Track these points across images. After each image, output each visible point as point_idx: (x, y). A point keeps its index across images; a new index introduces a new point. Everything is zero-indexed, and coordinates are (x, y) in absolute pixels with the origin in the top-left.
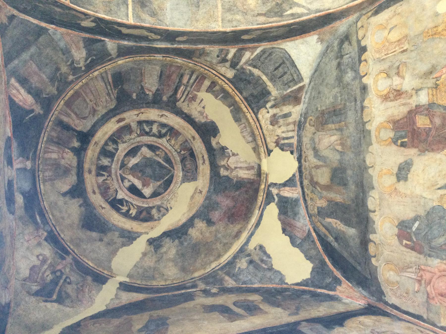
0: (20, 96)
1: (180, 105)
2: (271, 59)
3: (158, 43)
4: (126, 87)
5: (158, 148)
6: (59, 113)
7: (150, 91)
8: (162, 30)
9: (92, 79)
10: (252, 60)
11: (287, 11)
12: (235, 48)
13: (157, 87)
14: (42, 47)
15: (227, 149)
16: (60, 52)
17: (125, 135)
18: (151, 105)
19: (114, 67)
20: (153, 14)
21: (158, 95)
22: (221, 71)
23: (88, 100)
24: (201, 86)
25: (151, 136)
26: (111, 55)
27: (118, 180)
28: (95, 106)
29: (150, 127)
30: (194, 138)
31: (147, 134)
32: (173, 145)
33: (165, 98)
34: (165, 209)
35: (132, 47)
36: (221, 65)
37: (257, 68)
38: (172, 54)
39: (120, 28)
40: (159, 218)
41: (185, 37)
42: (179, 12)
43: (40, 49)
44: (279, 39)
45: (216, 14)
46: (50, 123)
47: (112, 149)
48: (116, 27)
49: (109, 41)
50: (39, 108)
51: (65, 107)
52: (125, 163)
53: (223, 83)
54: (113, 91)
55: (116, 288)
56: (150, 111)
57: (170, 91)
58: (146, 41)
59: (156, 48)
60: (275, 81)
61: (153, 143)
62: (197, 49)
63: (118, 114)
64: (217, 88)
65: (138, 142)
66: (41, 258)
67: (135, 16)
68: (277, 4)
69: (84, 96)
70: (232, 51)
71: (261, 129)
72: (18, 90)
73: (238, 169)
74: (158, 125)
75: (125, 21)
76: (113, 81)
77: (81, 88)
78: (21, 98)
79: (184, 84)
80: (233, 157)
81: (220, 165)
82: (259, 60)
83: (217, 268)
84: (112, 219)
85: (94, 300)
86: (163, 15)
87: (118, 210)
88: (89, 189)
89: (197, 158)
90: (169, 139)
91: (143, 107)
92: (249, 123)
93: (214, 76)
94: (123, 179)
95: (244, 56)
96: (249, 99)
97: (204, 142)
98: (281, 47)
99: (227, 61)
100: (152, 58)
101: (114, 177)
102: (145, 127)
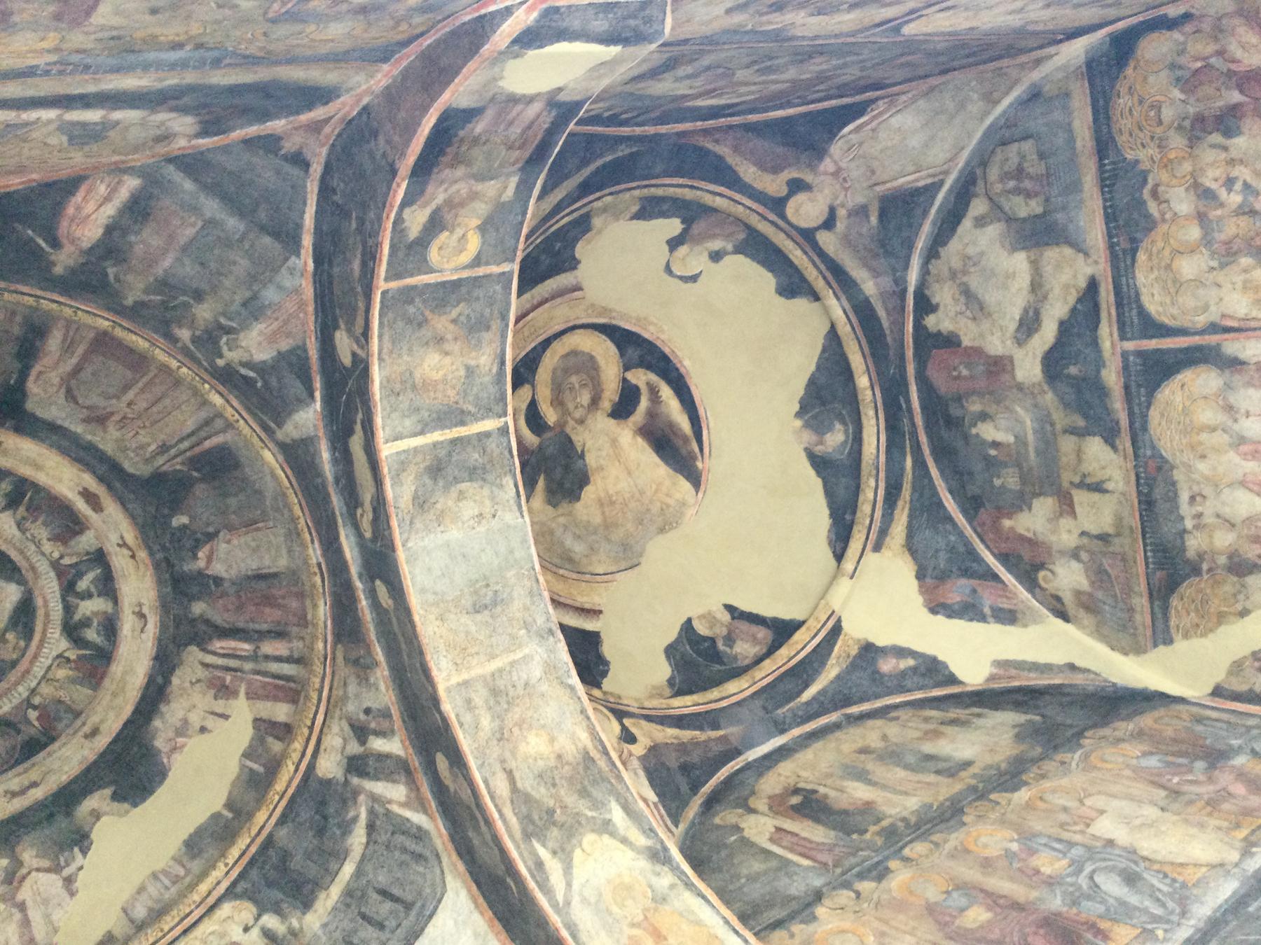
1: (191, 659)
2: (407, 865)
3: (352, 539)
4: (200, 490)
5: (28, 634)
6: (69, 323)
7: (209, 559)
8: (390, 534)
9: (196, 392)
10: (388, 813)
11: (544, 846)
12: (405, 748)
13: (224, 575)
15: (84, 852)
16: (248, 294)
17: (45, 524)
18: (167, 576)
19: (247, 442)
20: (421, 503)
21: (206, 584)
22: (329, 737)
23: (130, 395)
24: (267, 697)
25: (64, 599)
26: (280, 425)
28: (116, 418)
29: (93, 589)
30: (95, 732)
31: (69, 588)
32: (50, 676)
33: (198, 608)
35: (320, 474)
36: (347, 728)
37: (369, 835)
38: (335, 585)
39: (358, 427)
41: (390, 602)
42: (447, 566)
43: (241, 240)
44: (466, 863)
45: (475, 662)
46: (31, 299)
48: (360, 416)
49: (315, 411)
50: (71, 262)
51: (92, 335)
53: (295, 756)
54: (179, 460)
56: (144, 576)
57: (226, 615)
58: (347, 505)
59: (337, 538)
60: (348, 906)
61: (40, 613)
62: (368, 648)
63: (110, 487)
64: (276, 746)
65: (33, 568)
67: (403, 457)
68: (551, 812)
69: (140, 385)
70: (393, 746)
71: (185, 932)
72: (107, 199)
73: (18, 916)
74: (105, 613)
75: (380, 435)
76: (208, 452)
77: (165, 368)
79: (258, 647)
80: (60, 883)
81: (18, 849)
82: (393, 833)
86: (426, 527)
89: (26, 765)
90: (68, 660)
91: (151, 554)
92: (192, 887)
93: (309, 723)
95: (390, 785)
96: (271, 852)
97: (88, 770)
98: (449, 879)
99: (363, 742)
100: (307, 536)
102: (90, 576)
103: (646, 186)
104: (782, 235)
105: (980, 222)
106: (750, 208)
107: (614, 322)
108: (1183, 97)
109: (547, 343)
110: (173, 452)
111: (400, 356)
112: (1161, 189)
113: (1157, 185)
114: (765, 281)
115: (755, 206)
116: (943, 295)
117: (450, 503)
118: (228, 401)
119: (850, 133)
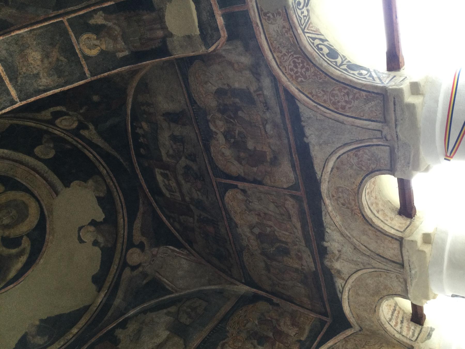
103: (115, 186)
104: (119, 256)
105: (168, 314)
106: (124, 236)
107: (47, 219)
108: (257, 323)
109: (27, 190)
111: (34, 40)
112: (227, 345)
113: (226, 343)
114: (95, 268)
115: (126, 237)
116: (132, 327)
119: (170, 249)
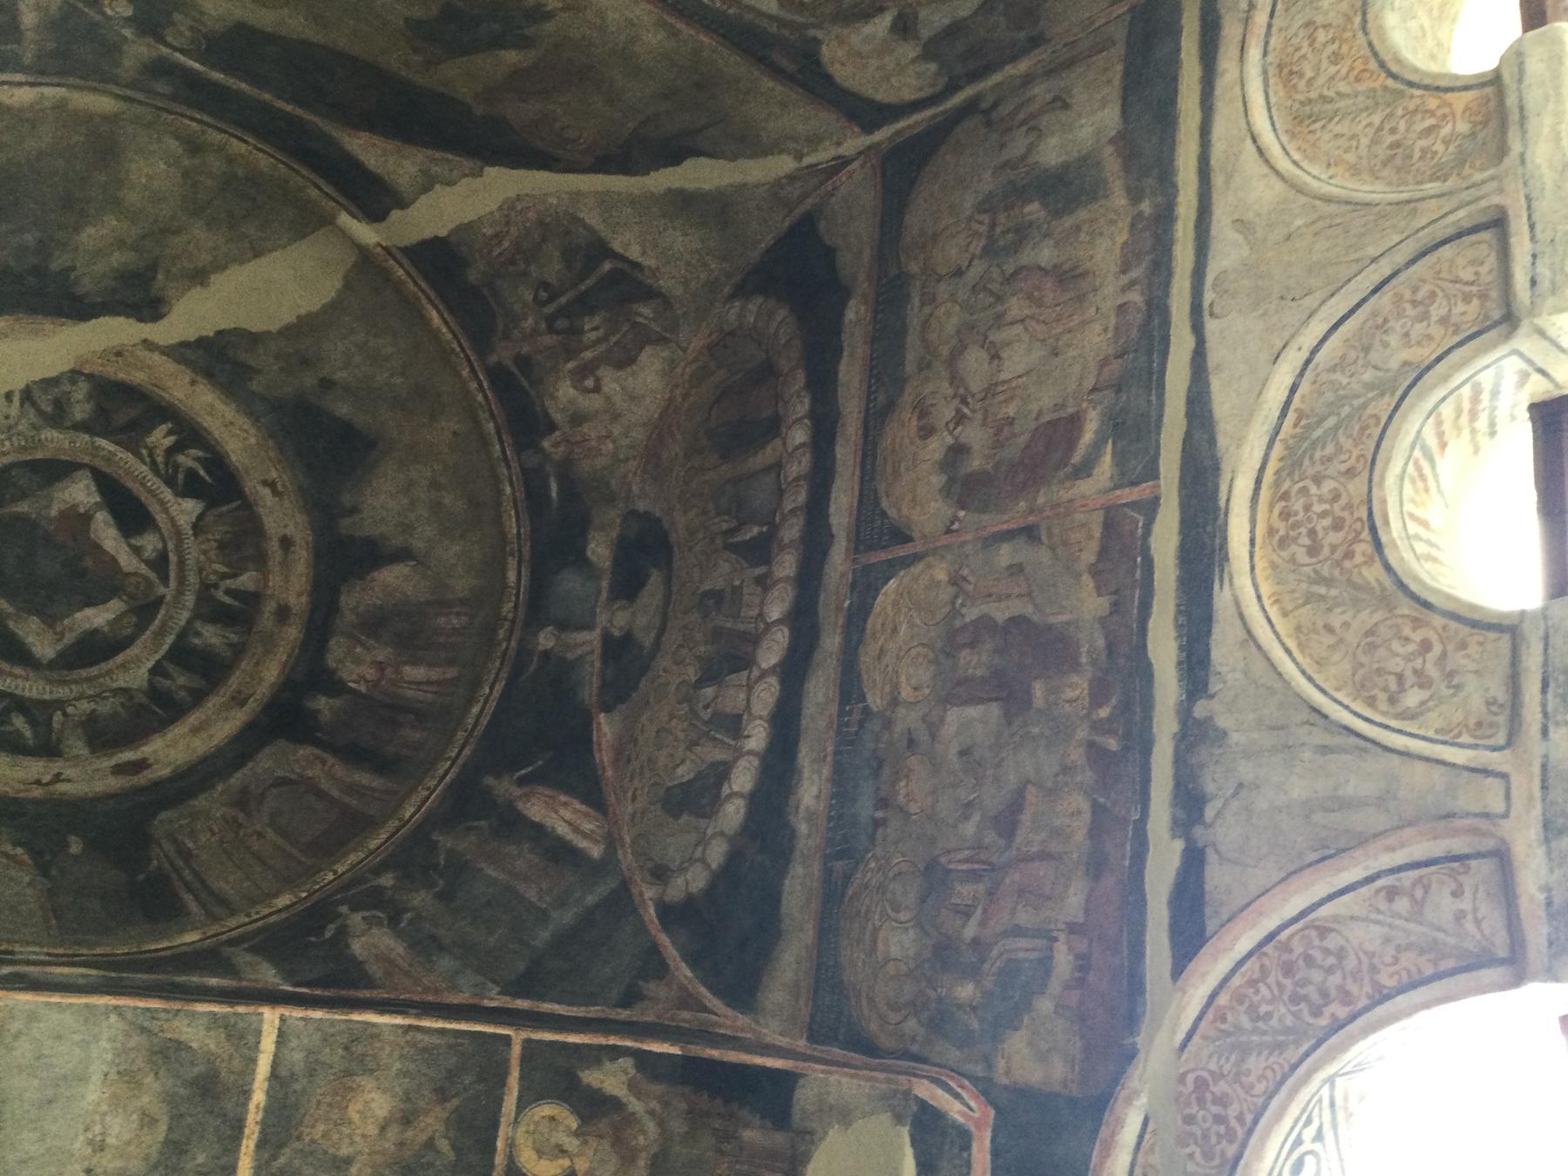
0: (567, 815)
3: (81, 981)
14: (511, 946)
20: (167, 1053)
27: (182, 563)
34: (34, 404)
40: (74, 382)
46: (453, 755)
47: (175, 675)
49: (278, 985)
52: (134, 619)
54: (166, 865)
55: (409, 211)
63: (140, 790)
65: (64, 682)
66: (590, 383)
67: (251, 1039)
72: (576, 830)
75: (286, 1011)
78: (562, 812)
83: (19, 77)
84: (253, 441)
85: (500, 208)
87: (217, 461)
88: (302, 558)
91: (36, 802)
94: (160, 563)
101: (193, 578)
110: (180, 863)
117: (145, 1099)
118: (280, 911)
